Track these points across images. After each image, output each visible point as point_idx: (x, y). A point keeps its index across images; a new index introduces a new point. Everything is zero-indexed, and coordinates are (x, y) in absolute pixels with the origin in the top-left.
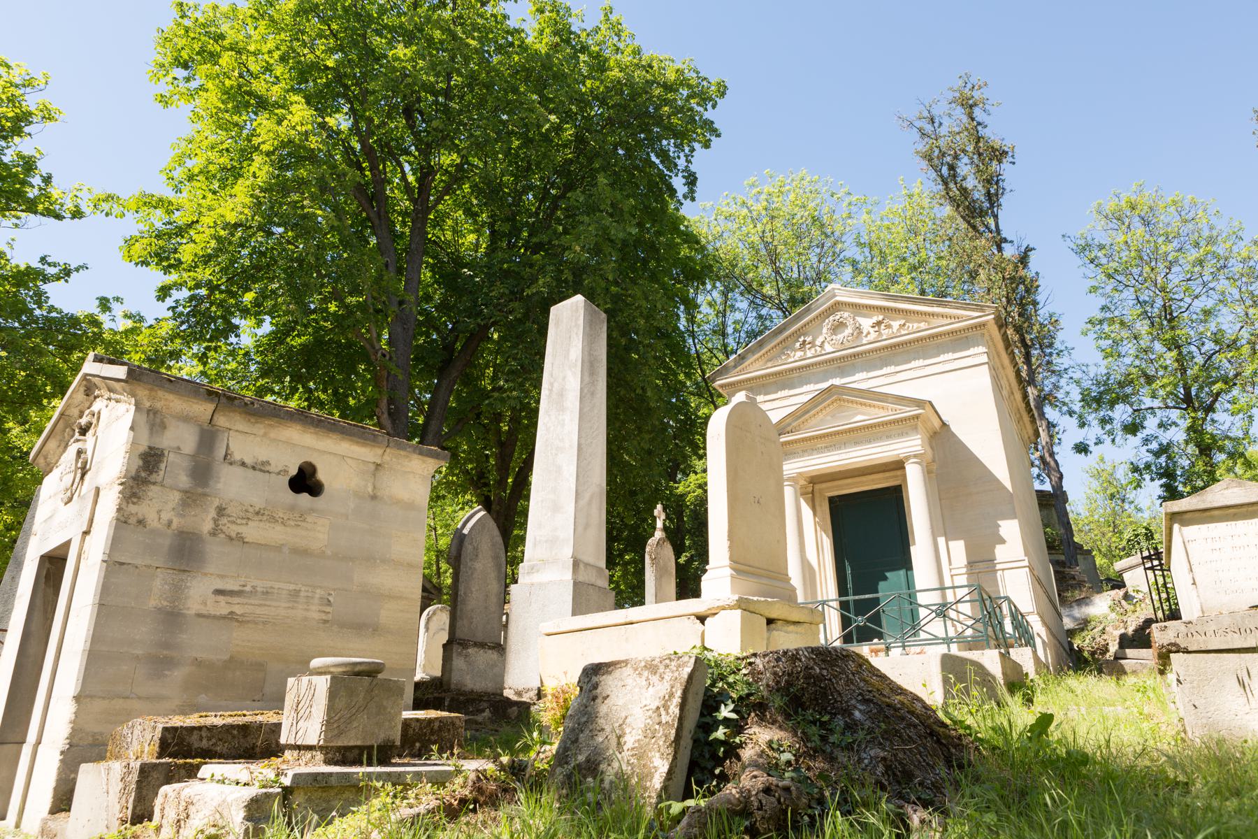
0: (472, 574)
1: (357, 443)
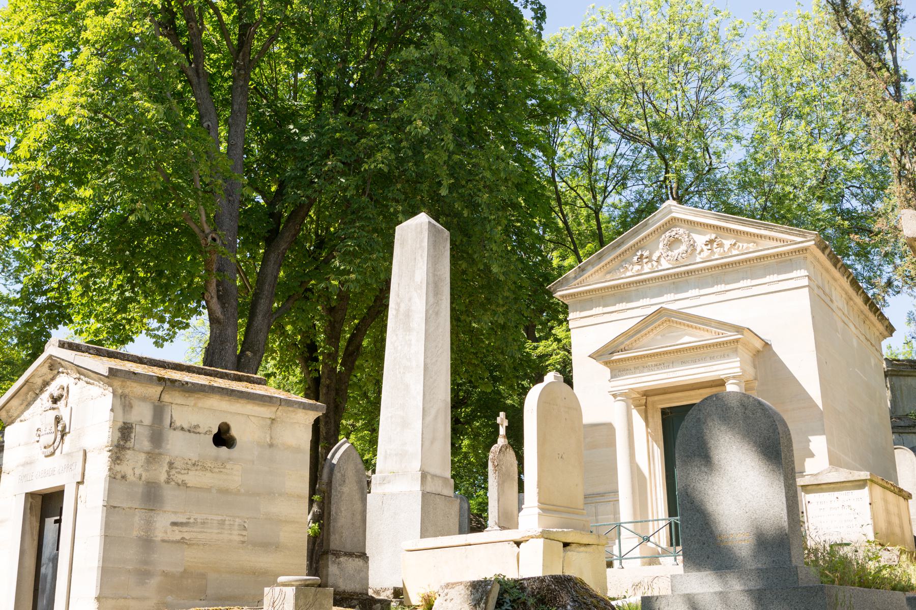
0: (341, 497)
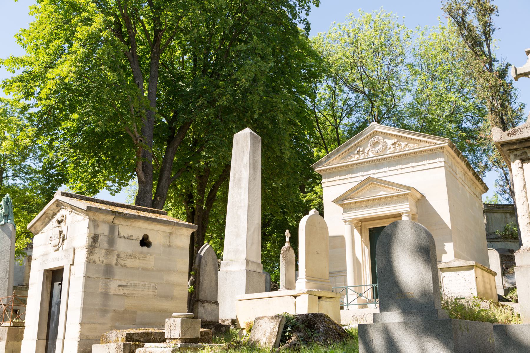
1: (163, 225)
